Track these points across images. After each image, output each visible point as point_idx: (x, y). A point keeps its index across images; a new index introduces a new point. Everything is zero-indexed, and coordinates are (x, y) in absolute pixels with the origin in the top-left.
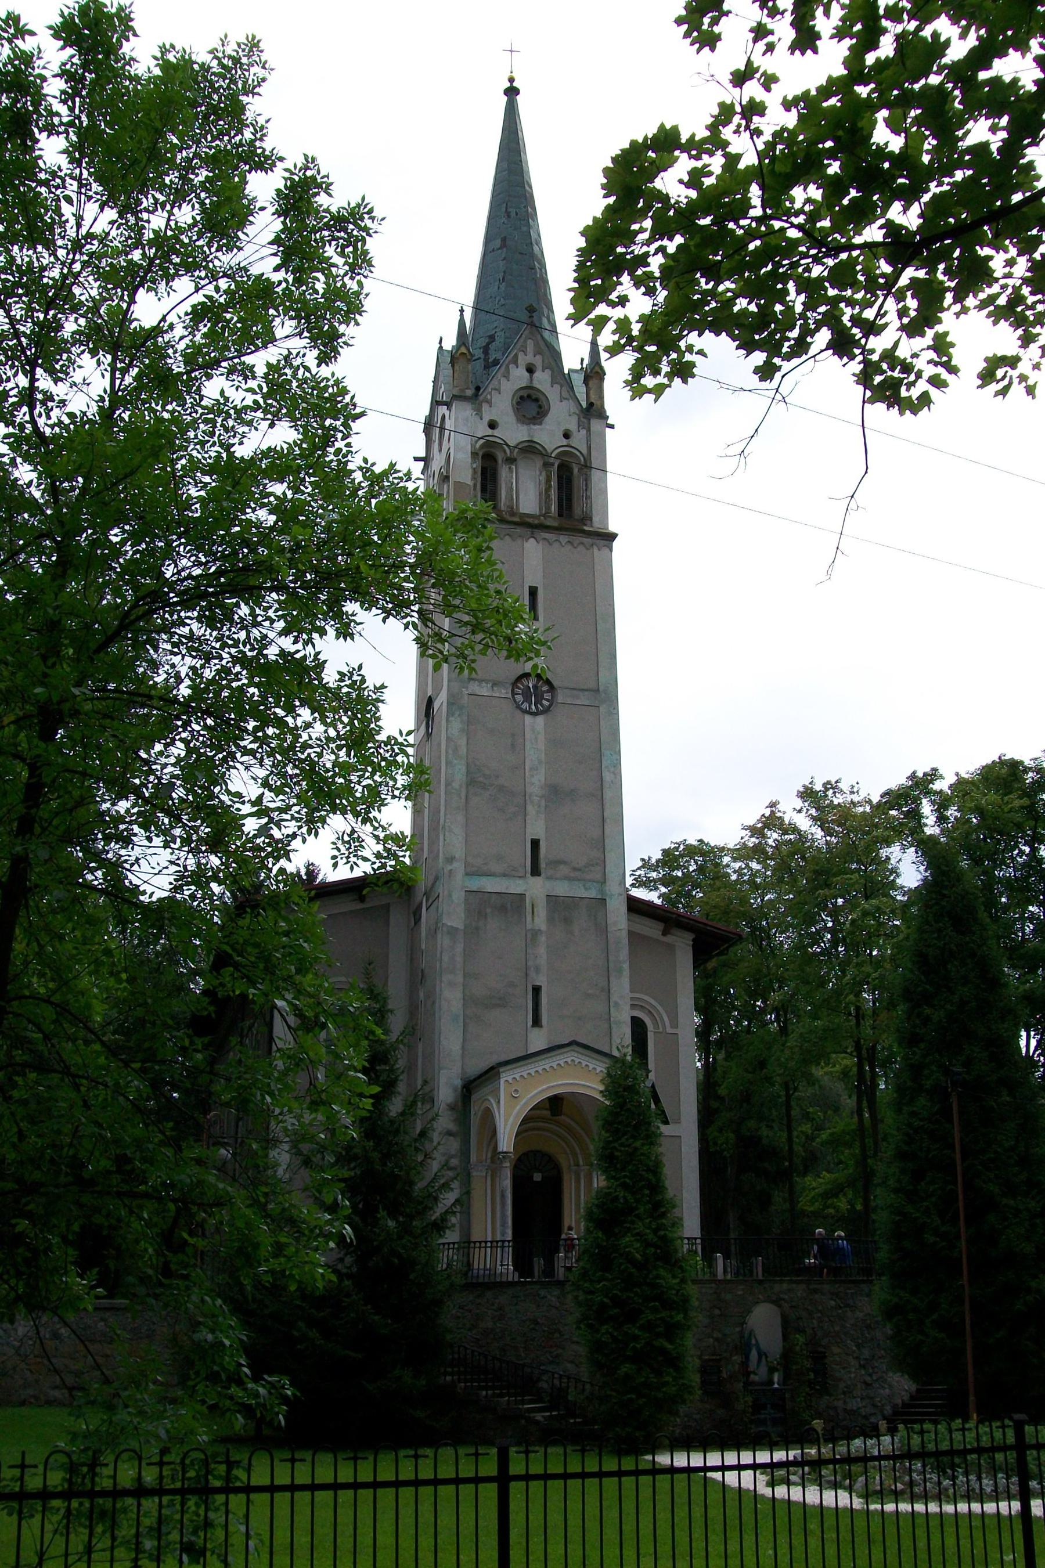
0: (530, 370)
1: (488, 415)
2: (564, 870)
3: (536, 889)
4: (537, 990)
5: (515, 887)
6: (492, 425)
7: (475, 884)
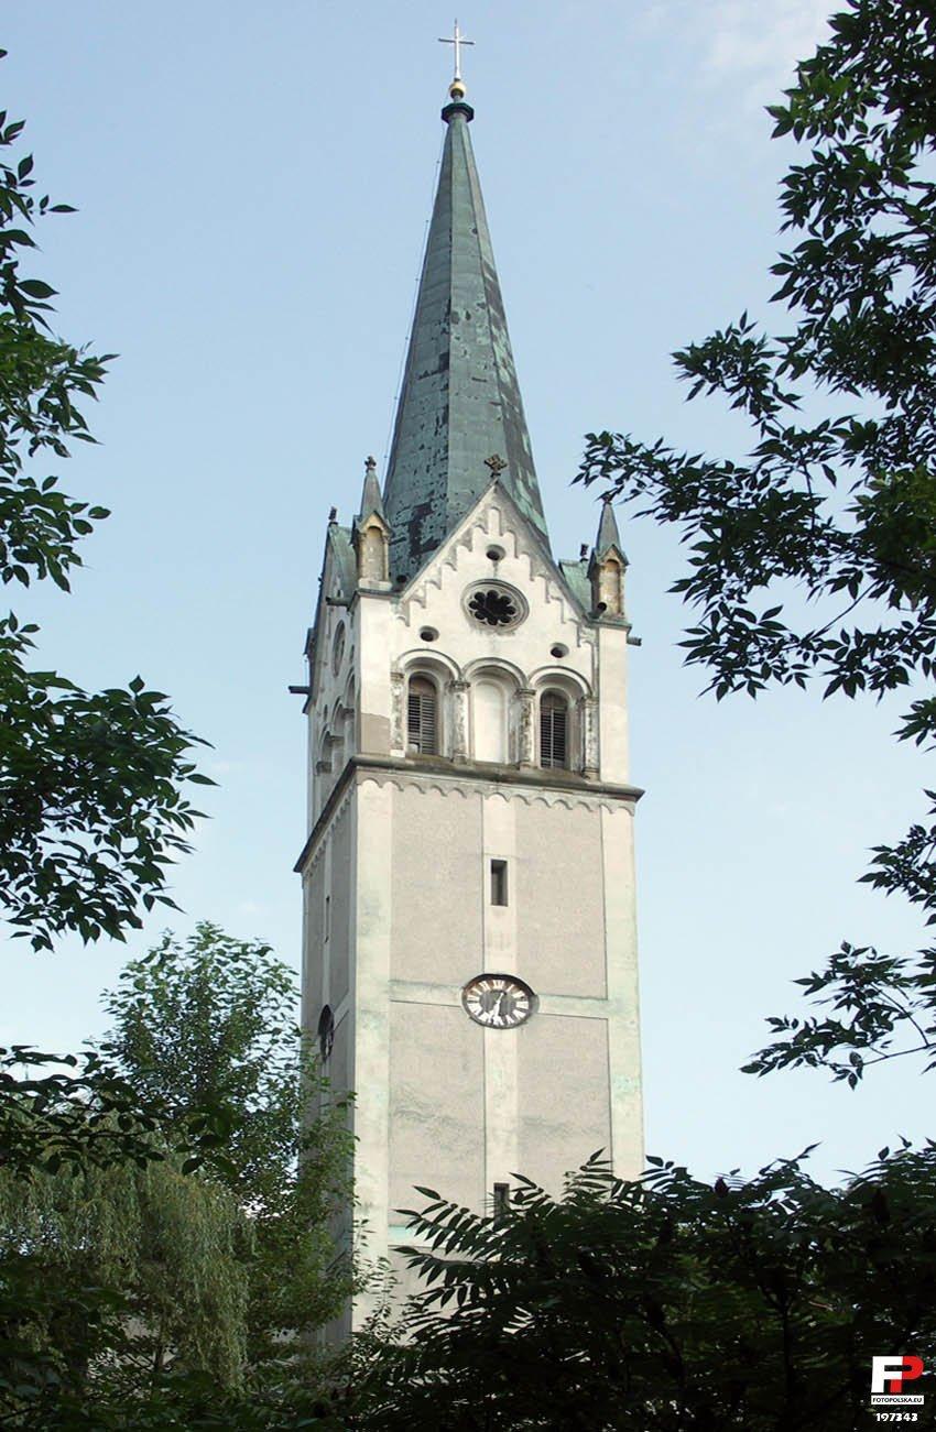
0: (494, 555)
1: (420, 619)
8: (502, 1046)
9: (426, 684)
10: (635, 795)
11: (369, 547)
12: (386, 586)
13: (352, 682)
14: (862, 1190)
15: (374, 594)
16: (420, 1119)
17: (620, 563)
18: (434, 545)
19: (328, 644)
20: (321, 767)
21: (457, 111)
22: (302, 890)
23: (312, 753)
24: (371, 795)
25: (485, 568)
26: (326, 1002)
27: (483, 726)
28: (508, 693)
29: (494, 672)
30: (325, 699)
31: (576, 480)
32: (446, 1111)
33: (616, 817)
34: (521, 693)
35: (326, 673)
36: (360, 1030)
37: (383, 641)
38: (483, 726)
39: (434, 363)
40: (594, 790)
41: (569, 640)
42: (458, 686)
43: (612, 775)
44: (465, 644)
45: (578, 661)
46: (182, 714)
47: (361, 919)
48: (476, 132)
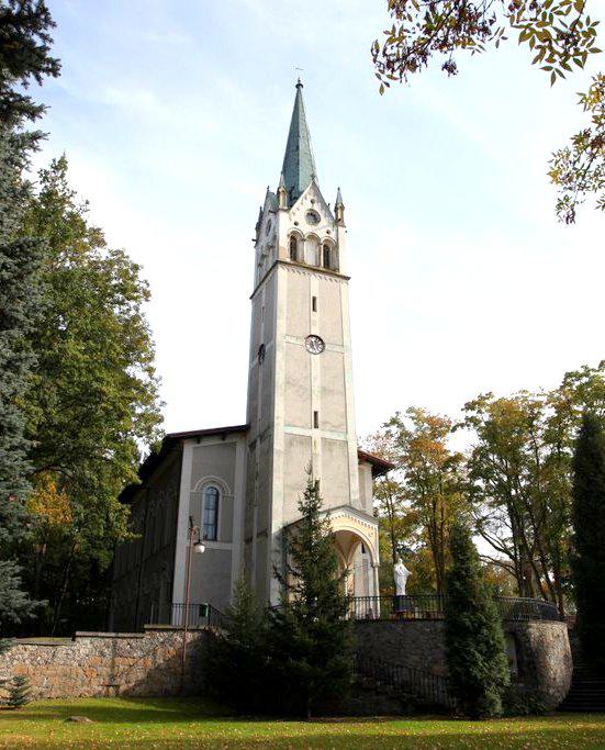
0: (312, 202)
1: (294, 219)
2: (328, 426)
3: (316, 434)
4: (314, 299)
5: (307, 433)
6: (296, 224)
7: (289, 430)
8: (316, 359)
9: (294, 240)
10: (348, 278)
11: (281, 197)
12: (286, 208)
13: (275, 238)
14: (54, 220)
15: (283, 210)
16: (293, 385)
17: (342, 208)
18: (296, 198)
19: (264, 227)
20: (259, 265)
21: (299, 86)
22: (249, 304)
23: (257, 260)
24: (282, 272)
25: (309, 206)
26: (262, 342)
27: (309, 254)
28: (315, 243)
29: (313, 237)
30: (263, 243)
31: (581, 94)
32: (301, 383)
33: (343, 284)
34: (319, 244)
35: (263, 235)
36: (278, 352)
37: (284, 225)
38: (309, 254)
39: (295, 148)
40: (339, 276)
41: (330, 229)
42: (304, 240)
43: (342, 272)
44: (306, 228)
45: (333, 235)
46: (134, 257)
47: (278, 313)
48: (303, 90)
